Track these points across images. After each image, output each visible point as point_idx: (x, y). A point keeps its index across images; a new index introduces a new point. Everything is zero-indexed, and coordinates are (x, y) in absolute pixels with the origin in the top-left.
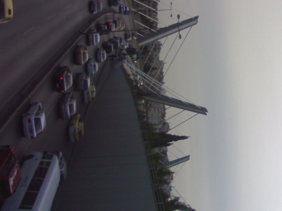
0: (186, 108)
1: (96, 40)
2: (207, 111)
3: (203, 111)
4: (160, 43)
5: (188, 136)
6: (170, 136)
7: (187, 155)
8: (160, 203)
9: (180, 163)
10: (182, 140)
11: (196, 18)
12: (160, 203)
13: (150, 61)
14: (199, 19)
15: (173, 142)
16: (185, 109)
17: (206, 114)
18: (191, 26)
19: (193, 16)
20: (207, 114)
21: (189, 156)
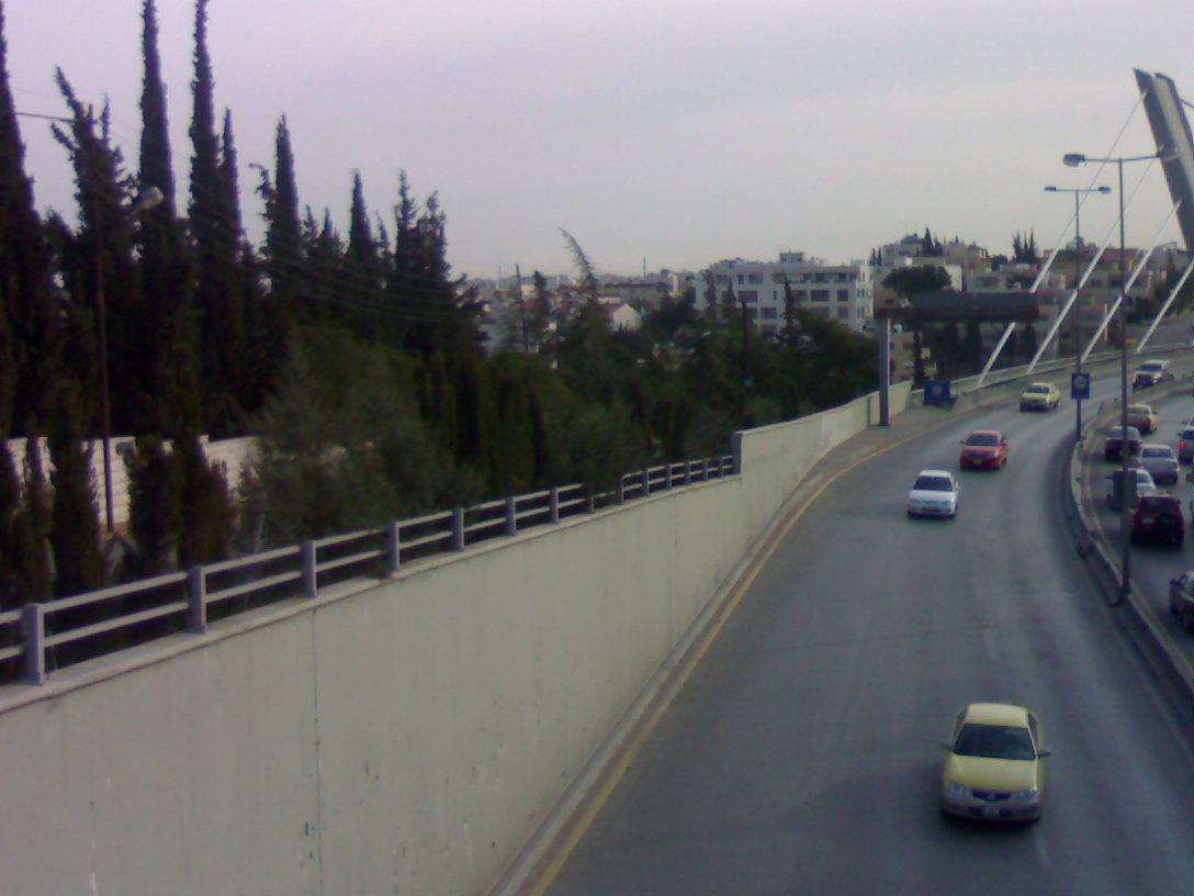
14: (1151, 69)
19: (1135, 95)
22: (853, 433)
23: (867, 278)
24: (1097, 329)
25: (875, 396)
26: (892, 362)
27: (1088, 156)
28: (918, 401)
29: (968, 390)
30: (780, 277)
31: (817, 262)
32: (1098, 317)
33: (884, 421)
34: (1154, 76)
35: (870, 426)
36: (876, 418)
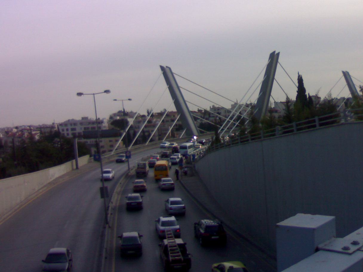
0: (271, 77)
1: (166, 182)
2: (274, 52)
3: (274, 58)
4: (212, 107)
5: (297, 75)
6: (298, 97)
7: (342, 74)
8: (317, 123)
9: (353, 83)
10: (304, 82)
11: (162, 68)
12: (317, 123)
13: (210, 122)
14: (164, 65)
15: (307, 93)
16: (273, 78)
17: (278, 54)
18: (172, 73)
19: (160, 72)
20: (275, 50)
21: (343, 72)
22: (65, 172)
23: (106, 123)
24: (166, 133)
25: (74, 161)
26: (306, 119)
27: (84, 93)
28: (92, 160)
29: (105, 157)
30: (81, 123)
31: (92, 119)
32: (168, 130)
33: (77, 168)
34: (165, 67)
35: (73, 169)
36: (75, 167)
